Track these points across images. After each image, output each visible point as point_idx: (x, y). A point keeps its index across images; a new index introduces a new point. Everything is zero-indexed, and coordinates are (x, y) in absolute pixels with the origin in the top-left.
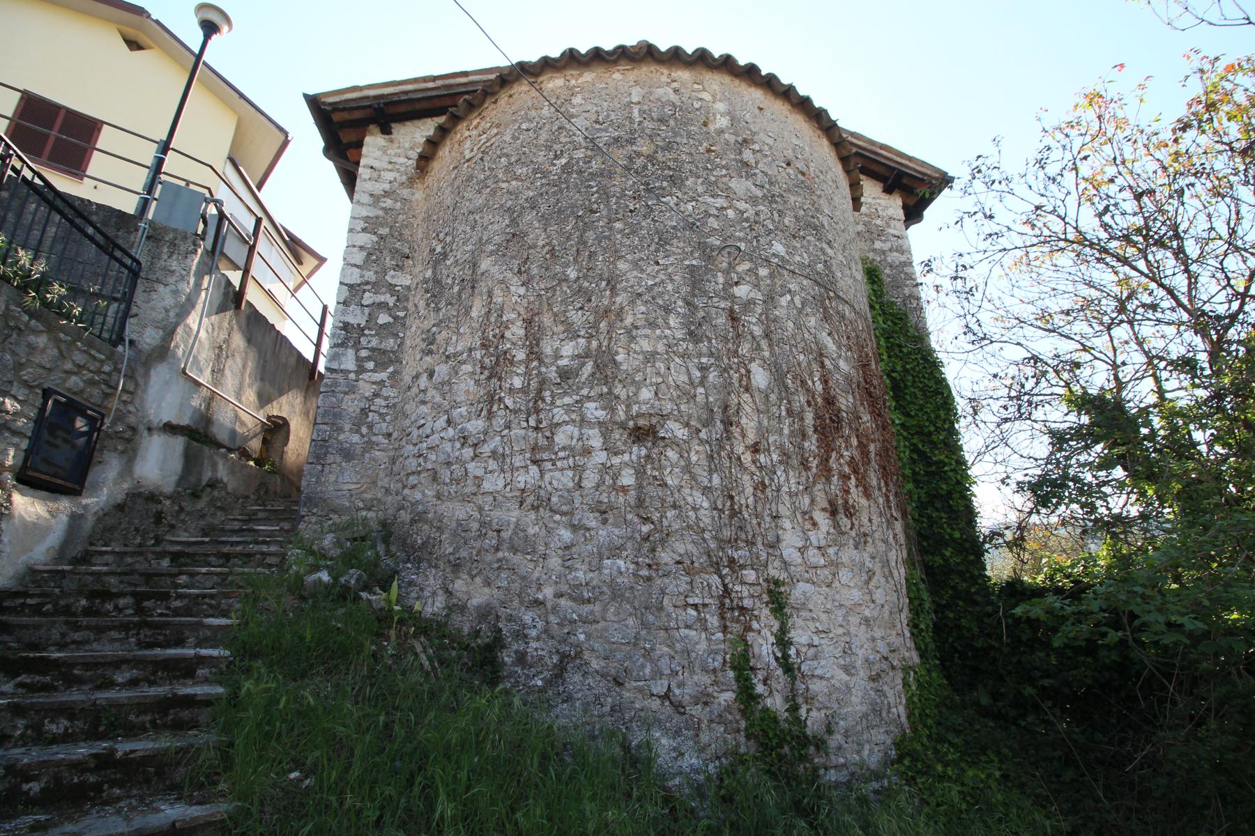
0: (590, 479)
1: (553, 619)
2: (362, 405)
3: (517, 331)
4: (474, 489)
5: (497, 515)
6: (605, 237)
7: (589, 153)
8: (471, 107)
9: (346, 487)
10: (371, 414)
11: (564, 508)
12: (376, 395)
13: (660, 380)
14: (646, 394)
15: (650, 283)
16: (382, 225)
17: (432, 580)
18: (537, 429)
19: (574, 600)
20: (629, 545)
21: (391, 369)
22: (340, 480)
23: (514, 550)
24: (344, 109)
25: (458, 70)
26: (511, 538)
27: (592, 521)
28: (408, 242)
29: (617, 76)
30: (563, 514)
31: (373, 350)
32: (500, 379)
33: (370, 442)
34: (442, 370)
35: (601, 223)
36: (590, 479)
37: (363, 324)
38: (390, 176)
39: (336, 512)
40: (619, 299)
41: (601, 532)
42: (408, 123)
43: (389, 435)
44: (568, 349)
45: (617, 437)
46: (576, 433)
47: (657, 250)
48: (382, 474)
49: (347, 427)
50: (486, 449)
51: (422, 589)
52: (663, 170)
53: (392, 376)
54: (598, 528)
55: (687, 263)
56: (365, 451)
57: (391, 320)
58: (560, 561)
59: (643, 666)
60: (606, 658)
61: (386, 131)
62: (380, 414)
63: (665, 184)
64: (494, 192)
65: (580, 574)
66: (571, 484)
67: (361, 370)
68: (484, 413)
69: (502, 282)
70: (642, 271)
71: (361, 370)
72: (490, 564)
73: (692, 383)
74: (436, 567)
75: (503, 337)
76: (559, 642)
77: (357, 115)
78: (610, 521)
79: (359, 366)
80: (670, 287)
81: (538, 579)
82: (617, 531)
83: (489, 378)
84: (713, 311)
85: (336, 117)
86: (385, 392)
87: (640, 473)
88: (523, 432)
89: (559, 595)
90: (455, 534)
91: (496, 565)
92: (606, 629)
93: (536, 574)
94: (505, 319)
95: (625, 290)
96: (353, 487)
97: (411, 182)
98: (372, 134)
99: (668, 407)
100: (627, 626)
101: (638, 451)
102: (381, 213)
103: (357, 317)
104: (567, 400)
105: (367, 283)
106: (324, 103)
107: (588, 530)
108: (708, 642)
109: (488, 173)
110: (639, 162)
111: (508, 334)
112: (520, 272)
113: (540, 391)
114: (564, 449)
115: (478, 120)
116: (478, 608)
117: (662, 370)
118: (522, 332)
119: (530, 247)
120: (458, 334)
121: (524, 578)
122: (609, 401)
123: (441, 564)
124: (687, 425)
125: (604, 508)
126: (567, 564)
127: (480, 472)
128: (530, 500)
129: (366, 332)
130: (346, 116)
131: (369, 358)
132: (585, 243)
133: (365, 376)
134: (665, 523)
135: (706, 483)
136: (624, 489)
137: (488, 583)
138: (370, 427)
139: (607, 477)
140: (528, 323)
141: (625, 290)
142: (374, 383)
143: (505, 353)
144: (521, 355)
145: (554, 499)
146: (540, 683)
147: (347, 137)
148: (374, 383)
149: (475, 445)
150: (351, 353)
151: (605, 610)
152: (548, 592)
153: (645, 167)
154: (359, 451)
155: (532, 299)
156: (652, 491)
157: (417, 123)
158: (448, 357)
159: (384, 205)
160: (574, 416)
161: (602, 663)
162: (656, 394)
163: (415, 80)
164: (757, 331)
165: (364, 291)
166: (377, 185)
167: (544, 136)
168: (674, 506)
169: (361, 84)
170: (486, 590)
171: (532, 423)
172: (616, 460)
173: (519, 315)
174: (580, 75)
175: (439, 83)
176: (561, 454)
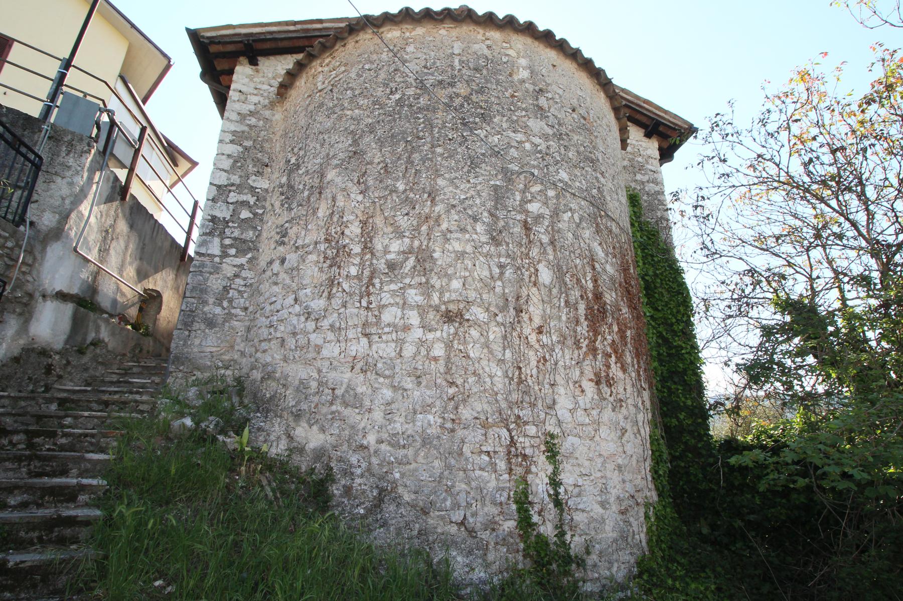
1: (375, 461)
2: (224, 283)
3: (355, 229)
5: (332, 375)
9: (208, 350)
11: (387, 373)
12: (236, 276)
14: (456, 284)
15: (463, 197)
16: (247, 139)
18: (367, 308)
19: (392, 446)
20: (438, 403)
21: (249, 255)
23: (346, 405)
24: (219, 43)
25: (315, 18)
26: (343, 396)
27: (409, 383)
30: (385, 377)
31: (235, 239)
32: (339, 267)
33: (229, 314)
34: (292, 258)
36: (409, 350)
37: (228, 218)
38: (255, 99)
39: (199, 369)
43: (246, 309)
44: (396, 246)
48: (238, 340)
49: (211, 301)
50: (325, 323)
51: (268, 435)
53: (250, 261)
54: (413, 389)
55: (492, 183)
56: (225, 321)
57: (251, 216)
58: (382, 414)
60: (416, 493)
61: (253, 62)
62: (239, 292)
63: (477, 120)
64: (340, 118)
67: (224, 255)
68: (325, 294)
69: (344, 190)
70: (457, 187)
71: (224, 255)
72: (325, 415)
74: (281, 417)
75: (343, 233)
77: (230, 48)
78: (424, 384)
79: (223, 252)
80: (478, 201)
85: (213, 49)
86: (244, 274)
87: (449, 346)
88: (357, 310)
89: (380, 441)
90: (298, 390)
91: (330, 417)
92: (416, 470)
93: (362, 425)
94: (345, 219)
95: (442, 201)
97: (272, 105)
98: (241, 64)
102: (246, 129)
103: (223, 212)
104: (393, 287)
105: (233, 185)
107: (406, 390)
110: (457, 101)
111: (347, 232)
112: (359, 182)
113: (371, 278)
117: (470, 266)
118: (359, 231)
119: (368, 163)
121: (353, 427)
122: (426, 288)
123: (285, 414)
127: (320, 342)
129: (230, 224)
130: (220, 48)
131: (231, 246)
132: (412, 162)
136: (436, 359)
138: (231, 301)
140: (364, 223)
141: (442, 201)
142: (234, 266)
144: (357, 249)
145: (380, 365)
147: (221, 65)
148: (234, 266)
150: (217, 240)
151: (416, 454)
152: (371, 439)
153: (462, 106)
154: (220, 320)
155: (368, 205)
159: (249, 122)
160: (398, 300)
161: (413, 496)
162: (464, 285)
165: (230, 191)
166: (244, 106)
170: (322, 436)
171: (364, 304)
172: (430, 336)
173: (357, 216)
174: (414, 29)
175: (299, 27)
176: (387, 330)
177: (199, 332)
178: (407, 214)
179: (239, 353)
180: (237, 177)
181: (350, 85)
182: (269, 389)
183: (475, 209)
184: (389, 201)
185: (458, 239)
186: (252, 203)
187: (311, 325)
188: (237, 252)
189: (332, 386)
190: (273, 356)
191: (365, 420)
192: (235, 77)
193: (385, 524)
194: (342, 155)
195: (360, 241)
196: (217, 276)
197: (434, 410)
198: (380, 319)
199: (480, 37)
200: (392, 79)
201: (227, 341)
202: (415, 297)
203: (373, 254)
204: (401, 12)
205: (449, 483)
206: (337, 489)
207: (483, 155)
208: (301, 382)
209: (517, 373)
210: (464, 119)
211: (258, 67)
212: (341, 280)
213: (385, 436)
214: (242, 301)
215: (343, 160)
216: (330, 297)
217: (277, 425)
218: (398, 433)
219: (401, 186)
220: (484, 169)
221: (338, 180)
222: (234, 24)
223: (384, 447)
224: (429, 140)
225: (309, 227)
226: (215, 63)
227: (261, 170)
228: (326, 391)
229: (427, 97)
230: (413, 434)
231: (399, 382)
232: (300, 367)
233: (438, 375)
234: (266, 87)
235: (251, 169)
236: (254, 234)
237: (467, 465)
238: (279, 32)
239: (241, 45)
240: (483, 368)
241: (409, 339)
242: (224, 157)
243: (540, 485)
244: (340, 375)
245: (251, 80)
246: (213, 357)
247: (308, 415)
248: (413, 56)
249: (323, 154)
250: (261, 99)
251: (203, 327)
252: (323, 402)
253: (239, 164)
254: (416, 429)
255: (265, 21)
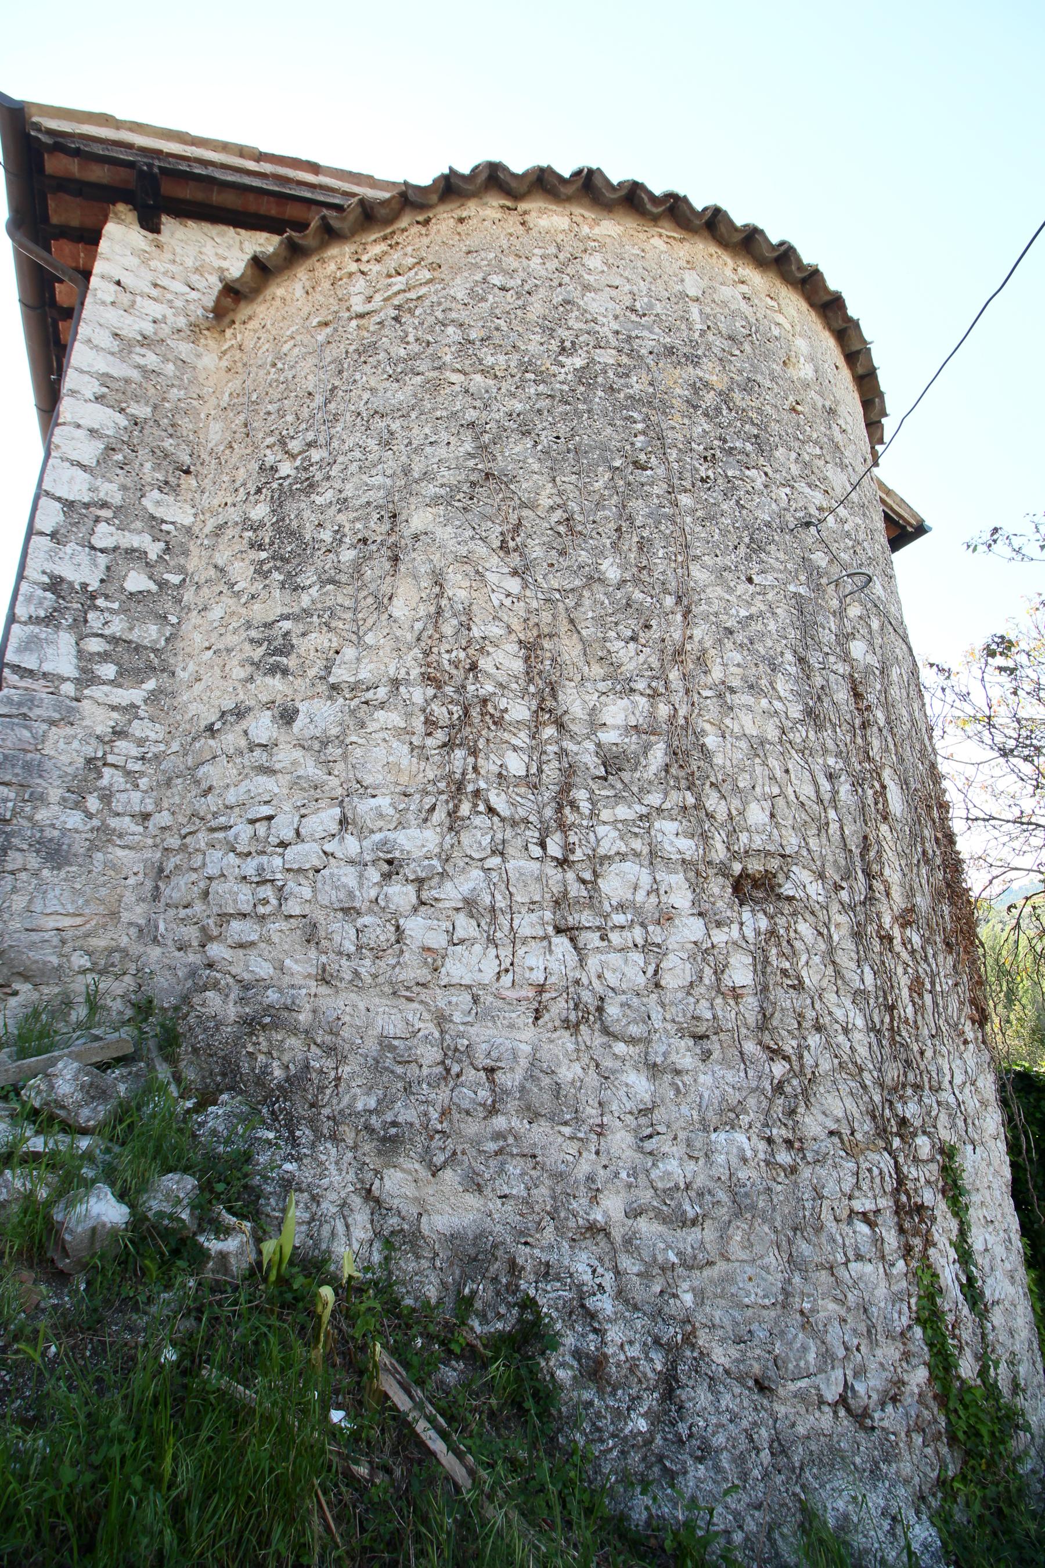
0: (677, 972)
1: (629, 1265)
2: (89, 751)
3: (505, 661)
4: (423, 974)
5: (484, 1037)
6: (666, 516)
7: (625, 360)
8: (331, 235)
9: (51, 923)
10: (106, 771)
11: (635, 1030)
12: (119, 733)
13: (776, 791)
14: (757, 815)
15: (743, 613)
16: (136, 398)
17: (335, 1174)
18: (563, 863)
19: (665, 1221)
20: (752, 1102)
21: (151, 684)
22: (38, 907)
23: (533, 1115)
24: (77, 153)
25: (304, 157)
26: (522, 1089)
27: (685, 1056)
28: (188, 443)
29: (656, 241)
30: (632, 1041)
31: (114, 640)
32: (474, 752)
33: (103, 829)
34: (320, 714)
35: (656, 490)
36: (677, 972)
37: (94, 585)
38: (157, 310)
39: (26, 977)
40: (697, 633)
41: (702, 1078)
42: (190, 223)
43: (146, 816)
44: (617, 713)
45: (716, 890)
46: (645, 880)
47: (748, 558)
48: (129, 898)
49: (55, 794)
50: (451, 893)
51: (315, 1199)
52: (744, 423)
53: (153, 698)
54: (696, 1071)
55: (792, 588)
56: (93, 847)
57: (154, 588)
58: (630, 1139)
59: (804, 1349)
60: (739, 1341)
61: (150, 224)
62: (128, 773)
63: (749, 447)
64: (434, 387)
65: (672, 1165)
66: (641, 980)
67: (87, 678)
68: (440, 815)
69: (466, 560)
70: (730, 590)
71: (87, 678)
72: (476, 1142)
73: (820, 801)
74: (335, 1138)
75: (473, 667)
76: (653, 1318)
77: (98, 174)
78: (716, 1055)
79: (84, 670)
80: (772, 626)
81: (590, 1179)
82: (730, 1076)
83: (448, 746)
84: (832, 677)
85: (55, 165)
86: (138, 729)
87: (761, 964)
88: (535, 866)
89: (634, 1213)
90: (377, 1067)
91: (491, 1146)
92: (728, 1279)
93: (584, 1168)
94: (476, 632)
95: (706, 618)
96: (67, 922)
97: (195, 330)
98: (121, 221)
99: (792, 842)
100: (766, 1269)
101: (753, 922)
102: (135, 375)
103: (80, 570)
104: (623, 812)
105: (104, 505)
106: (38, 127)
107: (678, 1072)
108: (881, 1283)
109: (415, 348)
110: (710, 399)
111: (484, 663)
112: (503, 547)
113: (566, 788)
114: (621, 907)
115: (382, 247)
116: (453, 1238)
117: (779, 773)
118: (518, 666)
119: (524, 505)
120: (359, 641)
121: (559, 1177)
122: (697, 819)
123: (349, 1136)
124: (821, 876)
125: (701, 1030)
126: (649, 1145)
127: (438, 940)
128: (559, 1008)
129: (100, 602)
130: (72, 167)
131: (104, 657)
132: (630, 519)
133: (97, 692)
134: (808, 1060)
135: (857, 984)
136: (735, 993)
137: (475, 1185)
138: (106, 798)
139: (707, 969)
140: (530, 649)
141: (706, 618)
142: (114, 708)
143: (485, 701)
144: (519, 711)
145: (613, 1010)
146: (643, 1425)
147: (63, 212)
148: (114, 708)
149: (420, 882)
150: (66, 640)
151: (724, 1238)
152: (611, 1207)
153: (718, 410)
154: (80, 846)
155: (535, 604)
156: (784, 999)
157: (207, 227)
158: (334, 687)
159: (142, 361)
160: (637, 845)
161: (734, 1352)
162: (772, 816)
163: (225, 147)
164: (882, 722)
165: (97, 520)
166: (129, 319)
167: (537, 308)
168: (819, 1028)
169: (120, 115)
170: (472, 1200)
171: (554, 849)
172: (719, 937)
173: (510, 630)
174: (596, 222)
175: (267, 168)
176: (619, 919)
177: (23, 876)
178: (632, 639)
179: (133, 931)
180: (114, 487)
181: (454, 315)
182: (280, 1056)
183: (769, 644)
184: (587, 602)
185: (750, 708)
186: (153, 556)
187: (401, 894)
188: (120, 674)
189: (488, 1063)
190: (273, 961)
191: (589, 1156)
192: (104, 245)
193: (705, 1453)
194: (448, 476)
195: (525, 692)
196: (69, 731)
197: (745, 1119)
198: (597, 890)
199: (728, 272)
200: (562, 321)
201: (102, 901)
202: (673, 837)
203: (561, 726)
204: (578, 173)
205: (807, 1306)
206: (563, 1365)
207: (768, 525)
208: (385, 1043)
209: (887, 1019)
210: (725, 441)
211: (160, 238)
212: (482, 785)
213: (646, 1196)
214: (136, 796)
215: (455, 489)
216: (454, 823)
217: (332, 1168)
218: (677, 1187)
219: (611, 571)
220: (774, 556)
221: (445, 533)
222: (119, 116)
223: (645, 1226)
224: (661, 471)
225: (369, 639)
226: (51, 204)
227: (172, 480)
228: (470, 1075)
229: (645, 378)
230: (711, 1185)
231: (665, 1055)
232: (380, 1004)
233: (743, 1031)
234: (180, 287)
235: (149, 472)
236: (159, 631)
237: (833, 1252)
238: (224, 167)
239: (124, 173)
240: (830, 1013)
241: (672, 943)
242: (81, 433)
243: (949, 1273)
244: (505, 1033)
245: (144, 263)
246: (63, 942)
247: (420, 1140)
248: (604, 280)
249: (391, 465)
250: (169, 312)
251: (34, 861)
252: (466, 1104)
253: (119, 457)
254: (715, 1172)
255: (195, 132)
